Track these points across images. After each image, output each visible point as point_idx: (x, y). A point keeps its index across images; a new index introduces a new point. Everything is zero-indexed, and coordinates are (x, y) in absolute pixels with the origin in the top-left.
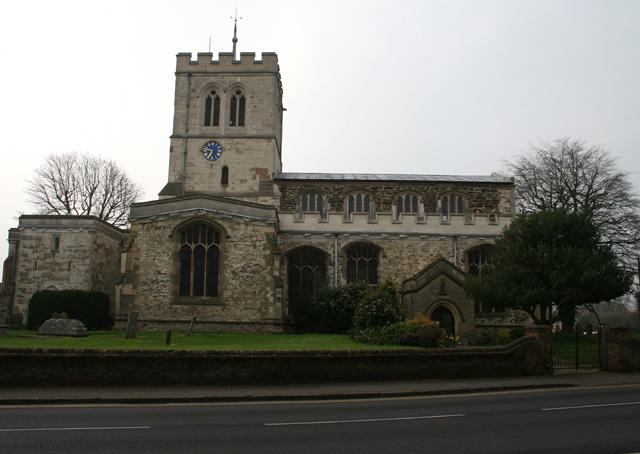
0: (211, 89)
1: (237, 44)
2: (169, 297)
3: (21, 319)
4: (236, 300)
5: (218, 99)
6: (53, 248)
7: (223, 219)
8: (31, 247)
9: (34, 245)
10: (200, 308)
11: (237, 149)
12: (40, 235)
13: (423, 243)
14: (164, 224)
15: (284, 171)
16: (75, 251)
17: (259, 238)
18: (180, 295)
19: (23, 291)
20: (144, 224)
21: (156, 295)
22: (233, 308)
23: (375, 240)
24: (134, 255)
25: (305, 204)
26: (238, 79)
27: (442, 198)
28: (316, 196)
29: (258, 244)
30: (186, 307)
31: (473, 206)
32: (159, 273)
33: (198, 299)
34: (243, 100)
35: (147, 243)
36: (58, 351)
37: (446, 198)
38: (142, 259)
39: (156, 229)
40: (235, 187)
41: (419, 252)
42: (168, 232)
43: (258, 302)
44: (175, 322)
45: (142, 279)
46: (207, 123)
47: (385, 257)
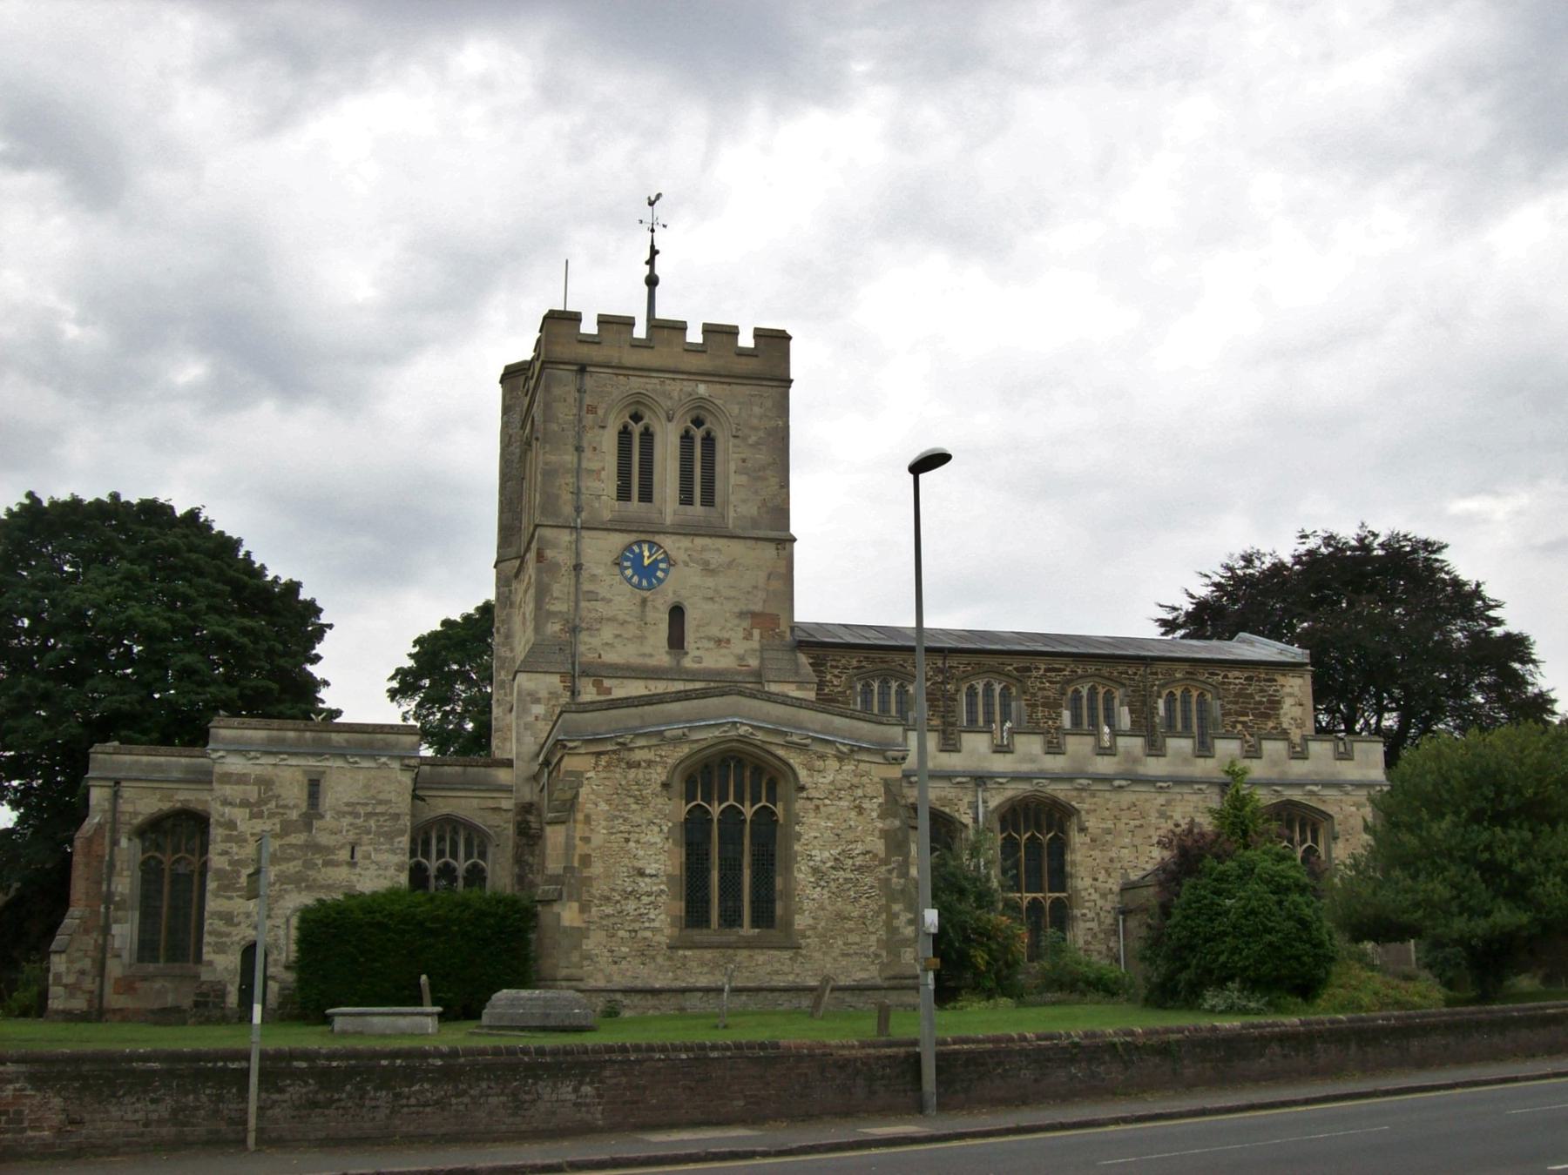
0: (632, 409)
1: (658, 289)
2: (667, 931)
3: (222, 994)
4: (823, 937)
5: (647, 436)
6: (304, 807)
7: (790, 745)
8: (245, 804)
9: (253, 798)
10: (743, 955)
11: (706, 563)
12: (269, 771)
13: (1161, 799)
14: (650, 755)
15: (796, 620)
16: (369, 815)
17: (870, 791)
18: (687, 926)
19: (228, 918)
20: (599, 754)
21: (636, 926)
22: (817, 955)
23: (1061, 791)
24: (580, 830)
25: (867, 702)
26: (702, 389)
27: (1165, 693)
28: (894, 685)
29: (866, 804)
30: (708, 955)
31: (1229, 714)
32: (641, 873)
33: (731, 935)
34: (709, 441)
35: (608, 802)
36: (997, 1040)
37: (1171, 694)
38: (597, 840)
39: (630, 765)
40: (702, 655)
41: (1153, 818)
42: (659, 775)
43: (873, 938)
44: (684, 991)
45: (600, 888)
46: (624, 494)
47: (1083, 830)
